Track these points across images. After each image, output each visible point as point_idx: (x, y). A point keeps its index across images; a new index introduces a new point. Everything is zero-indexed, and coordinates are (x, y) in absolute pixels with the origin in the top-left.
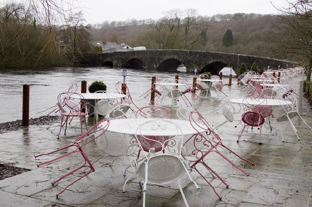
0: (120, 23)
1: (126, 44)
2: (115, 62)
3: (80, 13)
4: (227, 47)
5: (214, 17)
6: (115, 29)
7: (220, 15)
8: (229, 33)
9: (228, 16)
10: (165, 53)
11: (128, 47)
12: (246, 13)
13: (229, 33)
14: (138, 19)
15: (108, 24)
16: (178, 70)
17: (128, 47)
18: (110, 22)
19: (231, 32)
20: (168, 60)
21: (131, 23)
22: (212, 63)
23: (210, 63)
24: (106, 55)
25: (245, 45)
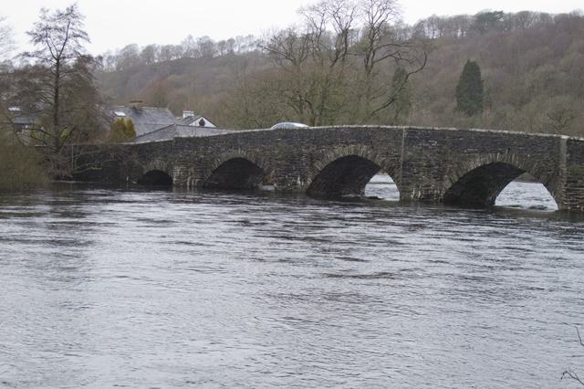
0: (166, 50)
1: (197, 114)
2: (177, 172)
3: (71, 11)
4: (470, 114)
5: (420, 25)
6: (154, 68)
8: (472, 71)
9: (460, 21)
10: (332, 138)
11: (202, 123)
12: (506, 11)
13: (472, 71)
14: (217, 37)
15: (135, 57)
16: (498, 203)
17: (202, 123)
18: (141, 46)
19: (478, 69)
20: (339, 161)
21: (196, 51)
22: (478, 168)
24: (147, 151)
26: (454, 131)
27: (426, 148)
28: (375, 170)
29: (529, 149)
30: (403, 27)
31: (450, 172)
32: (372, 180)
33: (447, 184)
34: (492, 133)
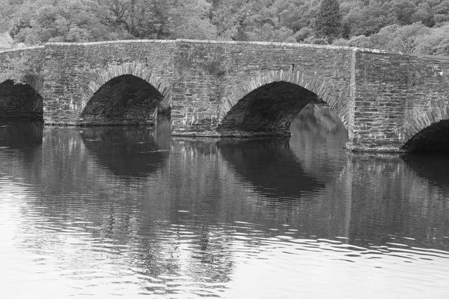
20: (115, 82)
34: (274, 47)
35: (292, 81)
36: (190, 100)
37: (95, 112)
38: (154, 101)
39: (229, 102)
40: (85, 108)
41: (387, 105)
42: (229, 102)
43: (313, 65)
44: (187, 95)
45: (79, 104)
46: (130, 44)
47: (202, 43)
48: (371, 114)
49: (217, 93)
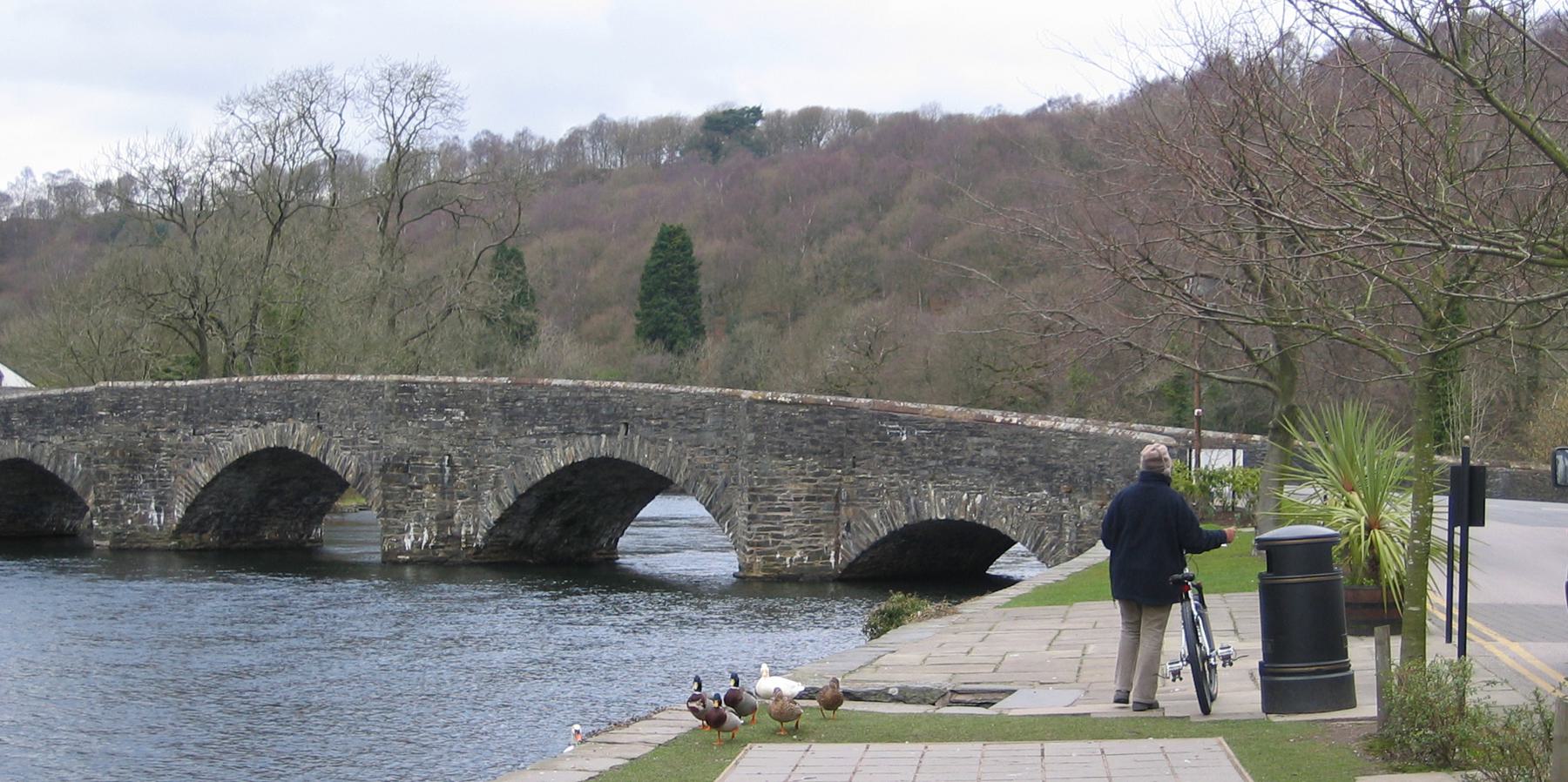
7: (614, 128)
12: (768, 108)
20: (246, 463)
21: (43, 205)
23: (547, 468)
25: (782, 328)
26: (505, 386)
27: (439, 427)
28: (659, 485)
29: (672, 423)
30: (533, 145)
31: (497, 482)
32: (645, 512)
33: (492, 512)
34: (588, 389)
35: (627, 457)
36: (419, 498)
37: (200, 528)
38: (322, 500)
39: (499, 502)
40: (183, 520)
41: (808, 498)
42: (499, 502)
43: (665, 426)
44: (413, 488)
45: (168, 512)
46: (279, 384)
47: (439, 384)
48: (779, 518)
49: (473, 482)
